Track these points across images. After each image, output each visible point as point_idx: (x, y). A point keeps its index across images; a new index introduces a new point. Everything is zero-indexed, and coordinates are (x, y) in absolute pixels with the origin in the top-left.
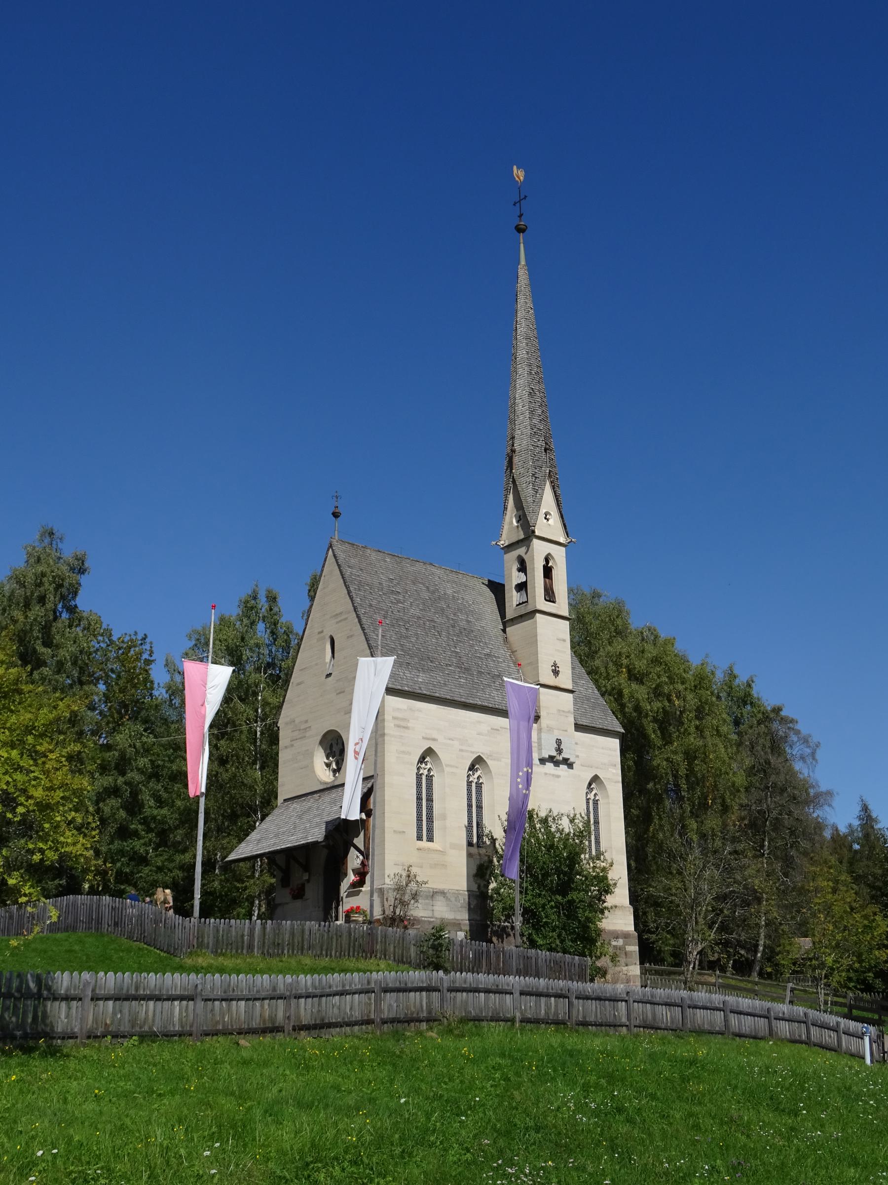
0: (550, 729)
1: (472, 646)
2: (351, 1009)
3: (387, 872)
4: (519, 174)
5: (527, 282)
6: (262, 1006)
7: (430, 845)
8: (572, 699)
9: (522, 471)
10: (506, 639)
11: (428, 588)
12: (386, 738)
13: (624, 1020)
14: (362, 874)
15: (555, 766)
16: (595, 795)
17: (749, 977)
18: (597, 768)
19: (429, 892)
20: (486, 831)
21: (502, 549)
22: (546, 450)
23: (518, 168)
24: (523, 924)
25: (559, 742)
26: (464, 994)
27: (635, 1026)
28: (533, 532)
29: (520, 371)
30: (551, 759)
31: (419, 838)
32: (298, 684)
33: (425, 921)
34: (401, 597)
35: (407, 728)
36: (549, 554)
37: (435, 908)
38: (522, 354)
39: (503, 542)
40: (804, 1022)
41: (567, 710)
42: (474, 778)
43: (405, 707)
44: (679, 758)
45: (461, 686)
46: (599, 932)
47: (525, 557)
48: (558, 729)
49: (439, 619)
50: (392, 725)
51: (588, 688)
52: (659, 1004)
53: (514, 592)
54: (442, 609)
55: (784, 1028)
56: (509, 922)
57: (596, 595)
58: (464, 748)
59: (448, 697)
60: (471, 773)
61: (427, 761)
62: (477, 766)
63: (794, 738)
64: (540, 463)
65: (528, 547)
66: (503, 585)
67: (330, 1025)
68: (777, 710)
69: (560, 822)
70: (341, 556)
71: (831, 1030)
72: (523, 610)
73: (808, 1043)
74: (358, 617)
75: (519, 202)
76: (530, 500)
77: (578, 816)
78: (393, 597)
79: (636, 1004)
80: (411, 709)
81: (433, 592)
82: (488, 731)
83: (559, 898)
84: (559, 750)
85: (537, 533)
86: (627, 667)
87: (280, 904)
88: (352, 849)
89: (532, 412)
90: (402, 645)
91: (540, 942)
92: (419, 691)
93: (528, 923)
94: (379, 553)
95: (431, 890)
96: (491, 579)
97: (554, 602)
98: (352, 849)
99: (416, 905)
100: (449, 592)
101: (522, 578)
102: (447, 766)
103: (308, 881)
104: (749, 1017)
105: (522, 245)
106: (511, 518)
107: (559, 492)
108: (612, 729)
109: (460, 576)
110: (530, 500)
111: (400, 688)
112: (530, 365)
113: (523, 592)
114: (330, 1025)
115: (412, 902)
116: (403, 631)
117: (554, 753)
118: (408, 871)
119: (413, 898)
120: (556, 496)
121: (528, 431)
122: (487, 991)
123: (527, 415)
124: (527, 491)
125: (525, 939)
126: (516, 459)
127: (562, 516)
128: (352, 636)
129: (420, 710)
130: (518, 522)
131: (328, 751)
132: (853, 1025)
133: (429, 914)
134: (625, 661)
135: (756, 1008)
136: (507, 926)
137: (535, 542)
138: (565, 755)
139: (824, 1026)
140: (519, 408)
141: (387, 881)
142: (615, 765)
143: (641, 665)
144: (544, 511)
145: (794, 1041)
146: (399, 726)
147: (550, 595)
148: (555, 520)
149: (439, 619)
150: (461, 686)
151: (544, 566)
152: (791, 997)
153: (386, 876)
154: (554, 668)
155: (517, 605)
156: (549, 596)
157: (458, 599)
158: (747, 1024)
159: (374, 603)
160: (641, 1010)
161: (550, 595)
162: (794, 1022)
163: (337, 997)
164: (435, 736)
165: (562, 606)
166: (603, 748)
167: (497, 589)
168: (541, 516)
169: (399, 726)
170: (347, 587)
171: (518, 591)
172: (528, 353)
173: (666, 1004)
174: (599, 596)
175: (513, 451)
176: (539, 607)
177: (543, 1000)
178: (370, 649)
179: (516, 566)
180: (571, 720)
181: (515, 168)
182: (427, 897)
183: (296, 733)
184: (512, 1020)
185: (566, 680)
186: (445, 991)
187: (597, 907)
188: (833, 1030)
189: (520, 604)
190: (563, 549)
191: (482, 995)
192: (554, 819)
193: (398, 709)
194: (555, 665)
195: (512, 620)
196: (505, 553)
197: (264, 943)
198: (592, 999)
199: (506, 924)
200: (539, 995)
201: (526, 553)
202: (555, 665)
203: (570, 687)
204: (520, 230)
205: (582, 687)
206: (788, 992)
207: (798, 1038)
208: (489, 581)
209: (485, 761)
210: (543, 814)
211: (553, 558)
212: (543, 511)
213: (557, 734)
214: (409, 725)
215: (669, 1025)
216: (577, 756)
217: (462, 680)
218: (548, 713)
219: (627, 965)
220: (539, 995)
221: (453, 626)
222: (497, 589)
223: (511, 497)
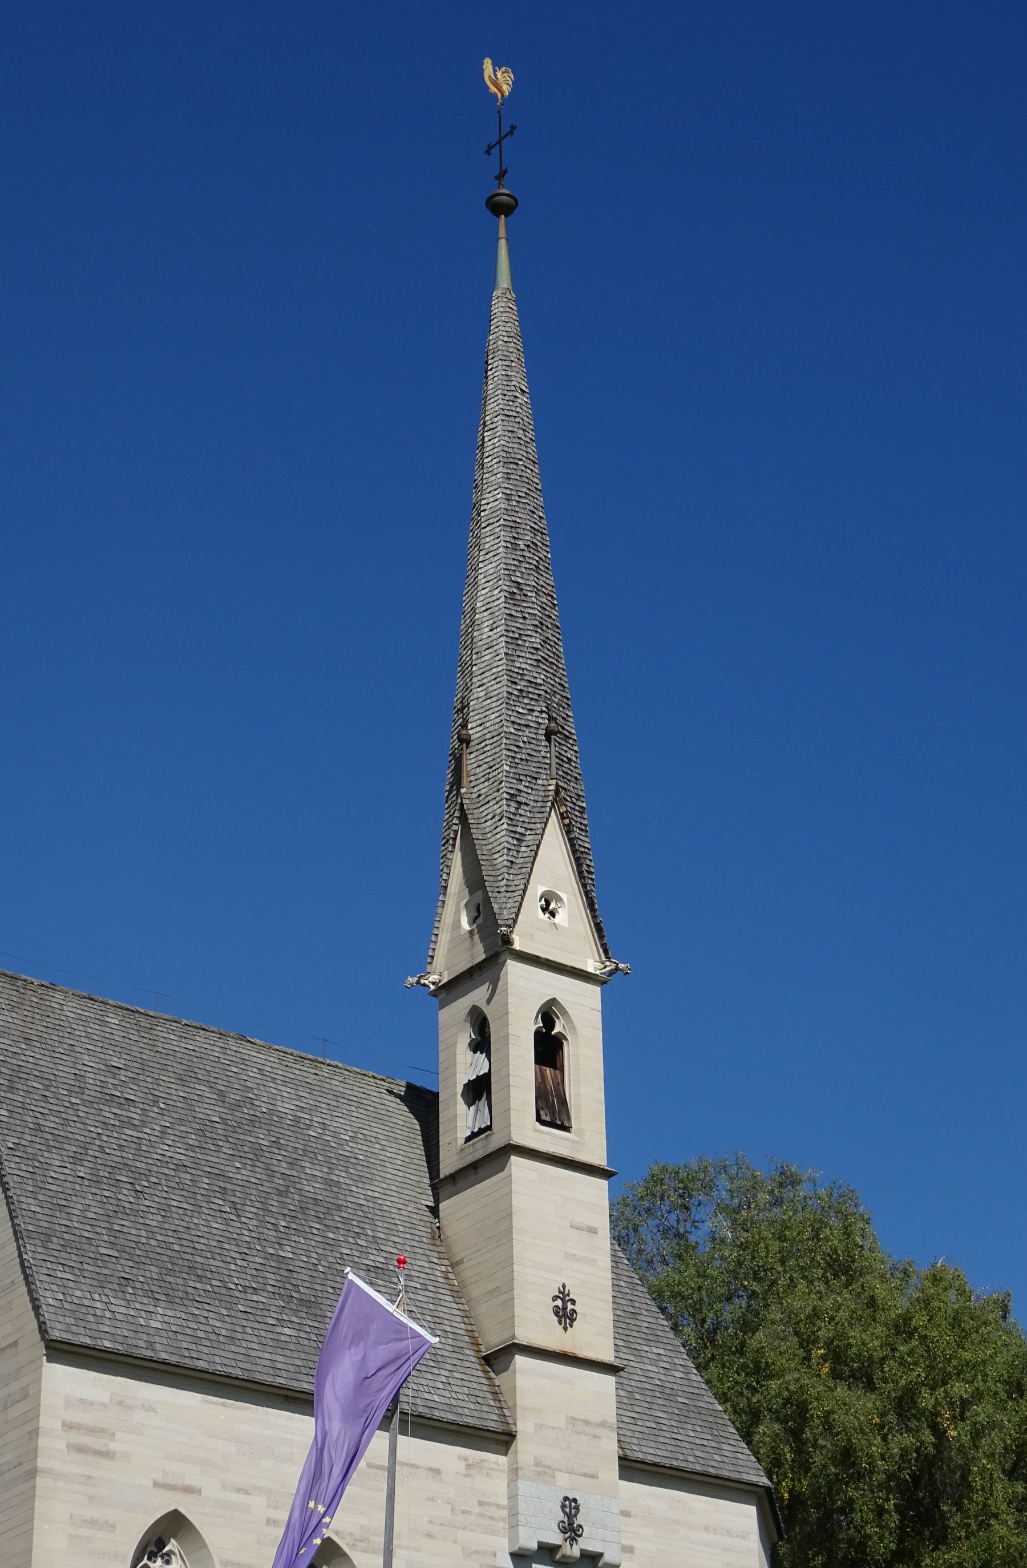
0: (544, 1471)
1: (333, 1245)
5: (513, 328)
8: (614, 1386)
9: (484, 788)
10: (437, 1234)
11: (221, 1094)
12: (40, 1481)
22: (548, 734)
23: (496, 65)
25: (570, 1507)
28: (507, 941)
29: (488, 543)
34: (135, 1114)
35: (107, 1455)
36: (553, 1002)
41: (598, 1421)
43: (105, 1398)
45: (281, 1346)
47: (488, 1011)
48: (571, 1472)
49: (240, 1173)
50: (61, 1445)
53: (461, 1105)
54: (258, 1150)
57: (789, 1180)
61: (169, 1554)
64: (532, 768)
65: (495, 983)
66: (436, 1095)
72: (480, 1149)
75: (499, 142)
76: (502, 860)
78: (108, 1112)
80: (120, 1403)
81: (238, 1105)
84: (571, 1530)
85: (517, 946)
89: (514, 641)
92: (149, 1353)
94: (90, 1003)
96: (418, 1083)
97: (567, 1129)
100: (286, 1107)
101: (479, 1065)
105: (503, 244)
106: (457, 913)
107: (585, 842)
108: (734, 1476)
110: (502, 860)
111: (88, 1341)
112: (514, 526)
113: (483, 1103)
116: (126, 1196)
117: (555, 1538)
120: (574, 852)
121: (502, 688)
123: (502, 648)
126: (471, 762)
127: (591, 905)
129: (149, 1408)
130: (473, 921)
137: (513, 969)
140: (483, 634)
144: (541, 889)
146: (81, 1449)
149: (240, 1173)
150: (281, 1346)
151: (538, 1033)
154: (559, 1303)
155: (468, 1139)
156: (553, 1113)
157: (309, 1127)
159: (50, 1123)
164: (192, 1479)
166: (706, 1529)
168: (532, 904)
169: (81, 1449)
171: (469, 1103)
172: (508, 498)
174: (794, 1182)
175: (465, 741)
176: (517, 1139)
178: (17, 1240)
179: (466, 1035)
180: (611, 1448)
181: (488, 64)
189: (473, 1135)
190: (597, 990)
193: (82, 1401)
195: (453, 1177)
196: (442, 1005)
201: (489, 1001)
203: (607, 1355)
204: (498, 208)
205: (654, 1362)
208: (409, 1087)
209: (344, 1554)
211: (564, 1012)
212: (537, 888)
213: (565, 1485)
214: (114, 1446)
216: (629, 1550)
217: (286, 1331)
218: (539, 1427)
223: (457, 860)
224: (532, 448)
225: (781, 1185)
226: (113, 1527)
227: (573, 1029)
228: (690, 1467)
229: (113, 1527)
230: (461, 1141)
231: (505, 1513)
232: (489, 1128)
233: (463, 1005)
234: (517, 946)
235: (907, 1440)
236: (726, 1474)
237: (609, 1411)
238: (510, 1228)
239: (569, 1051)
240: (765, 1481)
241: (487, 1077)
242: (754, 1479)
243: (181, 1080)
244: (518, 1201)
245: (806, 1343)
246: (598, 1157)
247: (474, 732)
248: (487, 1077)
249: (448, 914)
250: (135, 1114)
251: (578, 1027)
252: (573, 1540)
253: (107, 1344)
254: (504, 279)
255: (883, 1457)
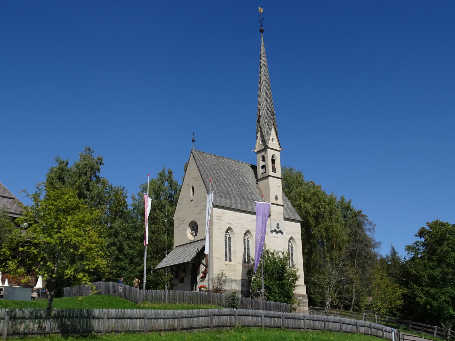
0: (275, 220)
1: (245, 189)
2: (202, 322)
3: (214, 273)
4: (261, 10)
6: (169, 321)
7: (230, 262)
9: (263, 123)
11: (228, 167)
13: (303, 326)
14: (205, 273)
15: (276, 233)
16: (292, 244)
17: (349, 311)
18: (292, 234)
19: (230, 280)
20: (251, 258)
21: (256, 153)
22: (272, 115)
24: (265, 291)
25: (278, 224)
26: (244, 317)
27: (307, 329)
28: (268, 146)
29: (262, 85)
30: (275, 231)
31: (226, 260)
32: (180, 204)
33: (228, 291)
34: (218, 171)
35: (221, 220)
36: (274, 154)
37: (232, 286)
38: (263, 79)
39: (256, 150)
40: (370, 327)
41: (280, 213)
42: (246, 238)
44: (323, 230)
45: (241, 204)
46: (293, 294)
47: (265, 156)
49: (232, 179)
50: (216, 219)
51: (289, 204)
52: (315, 321)
53: (261, 169)
54: (234, 176)
55: (362, 329)
56: (259, 291)
58: (242, 227)
59: (236, 208)
60: (245, 236)
62: (247, 234)
63: (366, 222)
64: (270, 120)
65: (266, 152)
67: (194, 328)
68: (360, 212)
69: (278, 254)
70: (195, 155)
71: (380, 330)
72: (264, 175)
73: (371, 335)
74: (202, 178)
76: (266, 134)
77: (285, 252)
78: (215, 171)
79: (307, 320)
80: (222, 213)
81: (230, 169)
82: (251, 221)
83: (278, 282)
84: (278, 228)
85: (269, 147)
86: (303, 196)
87: (175, 285)
88: (201, 264)
89: (267, 101)
90: (219, 189)
91: (271, 298)
92: (226, 206)
93: (267, 291)
95: (231, 279)
97: (276, 172)
98: (201, 264)
99: (225, 285)
100: (236, 169)
101: (263, 163)
102: (236, 233)
103: (185, 276)
104: (349, 325)
105: (262, 37)
106: (259, 141)
107: (277, 131)
109: (240, 163)
111: (218, 205)
112: (266, 83)
113: (264, 169)
114: (194, 328)
115: (224, 284)
116: (219, 184)
117: (276, 229)
118: (222, 272)
119: (224, 282)
120: (276, 132)
122: (252, 316)
124: (265, 131)
125: (265, 297)
126: (261, 119)
127: (278, 140)
128: (200, 186)
129: (226, 213)
130: (262, 142)
131: (192, 229)
132: (388, 328)
133: (230, 288)
134: (302, 194)
135: (349, 322)
136: (259, 292)
137: (268, 150)
138: (280, 229)
139: (377, 329)
140: (262, 99)
141: (214, 276)
142: (299, 233)
143: (308, 196)
144: (272, 138)
145: (366, 334)
146: (218, 219)
147: (274, 170)
148: (276, 142)
149: (232, 179)
150: (241, 204)
152: (365, 318)
153: (214, 274)
155: (262, 174)
157: (240, 172)
158: (349, 328)
159: (208, 173)
160: (309, 323)
161: (274, 170)
162: (366, 327)
163: (197, 318)
165: (279, 174)
166: (294, 227)
167: (254, 168)
170: (198, 168)
172: (265, 78)
173: (318, 321)
175: (260, 116)
176: (270, 174)
177: (273, 319)
179: (261, 159)
180: (282, 216)
181: (259, 7)
182: (229, 282)
183: (180, 222)
184: (261, 326)
185: (280, 201)
186: (236, 316)
187: (292, 285)
188: (381, 330)
189: (263, 173)
191: (250, 317)
192: (276, 253)
193: (218, 213)
194: (276, 196)
196: (257, 154)
197: (169, 299)
198: (291, 319)
199: (259, 292)
200: (271, 317)
201: (265, 154)
202: (276, 196)
203: (282, 204)
204: (261, 31)
205: (286, 204)
206: (364, 317)
207: (367, 333)
208: (251, 165)
210: (272, 251)
212: (271, 138)
213: (277, 222)
214: (222, 218)
215: (319, 328)
216: (285, 230)
219: (303, 307)
220: (271, 317)
221: (238, 182)
222: (254, 168)
223: (259, 133)
224: (268, 70)
225: (290, 170)
226: (222, 229)
227: (276, 158)
228: (292, 219)
229: (222, 229)
230: (261, 174)
231: (269, 226)
232: (265, 172)
233: (261, 154)
234: (269, 147)
235: (315, 210)
236: (297, 219)
237: (282, 211)
238: (269, 187)
239: (275, 161)
240: (302, 220)
241: (265, 165)
242: (300, 220)
243: (223, 166)
244: (270, 183)
245: (300, 196)
246: (280, 176)
247: (261, 114)
248: (265, 165)
249: (258, 141)
250: (218, 171)
251: (277, 158)
252: (278, 229)
253: (221, 205)
254: (263, 44)
255: (312, 213)
